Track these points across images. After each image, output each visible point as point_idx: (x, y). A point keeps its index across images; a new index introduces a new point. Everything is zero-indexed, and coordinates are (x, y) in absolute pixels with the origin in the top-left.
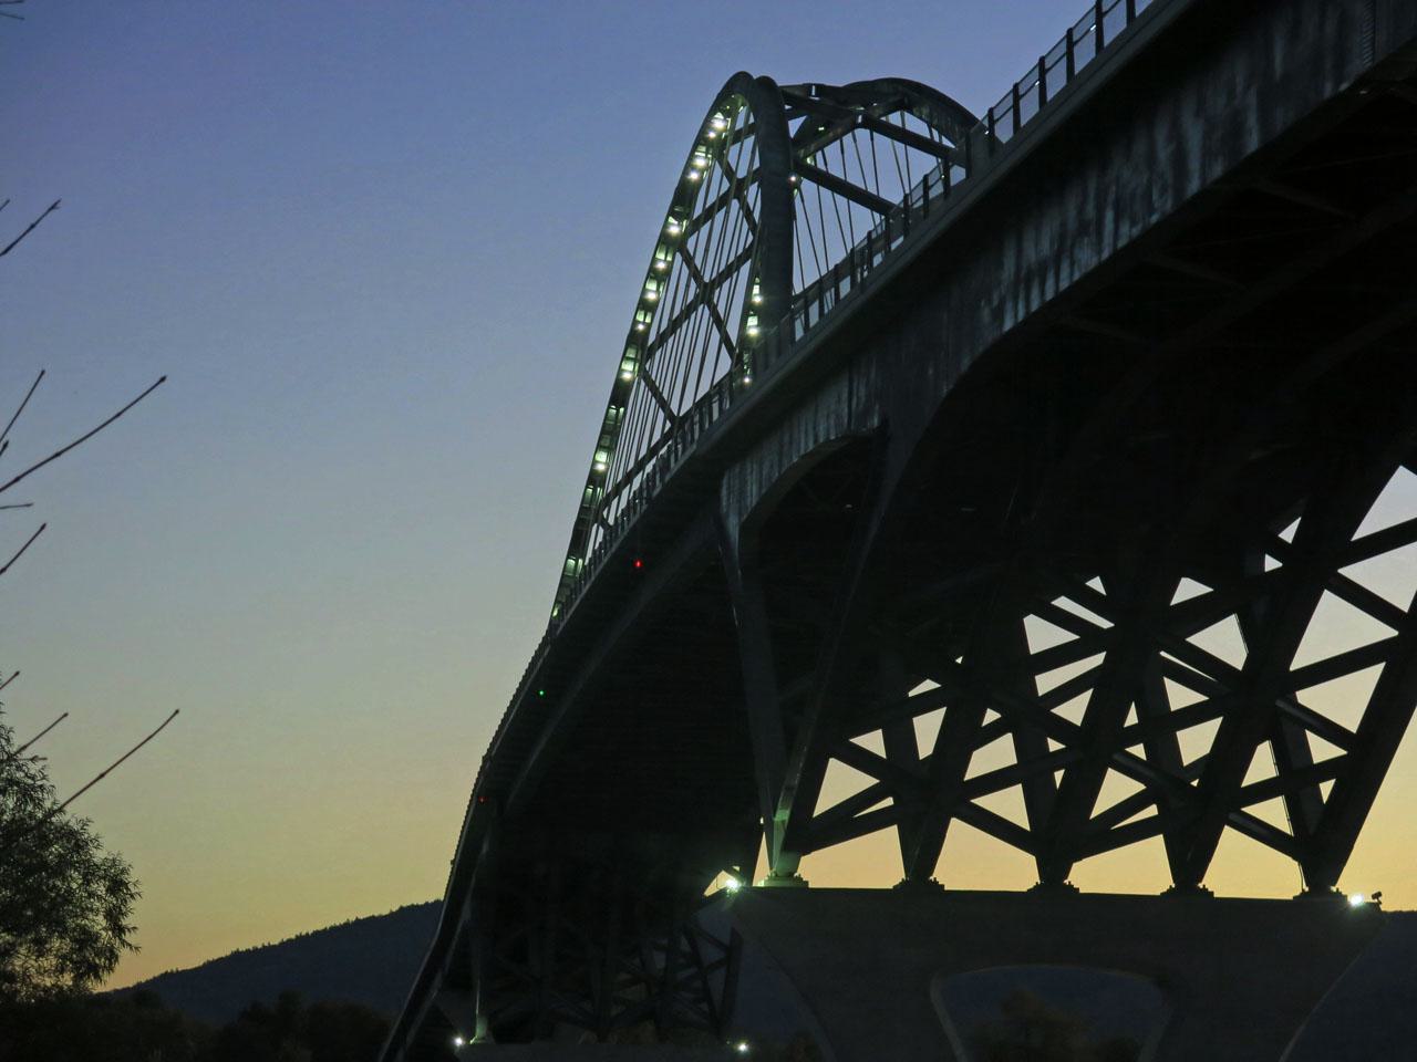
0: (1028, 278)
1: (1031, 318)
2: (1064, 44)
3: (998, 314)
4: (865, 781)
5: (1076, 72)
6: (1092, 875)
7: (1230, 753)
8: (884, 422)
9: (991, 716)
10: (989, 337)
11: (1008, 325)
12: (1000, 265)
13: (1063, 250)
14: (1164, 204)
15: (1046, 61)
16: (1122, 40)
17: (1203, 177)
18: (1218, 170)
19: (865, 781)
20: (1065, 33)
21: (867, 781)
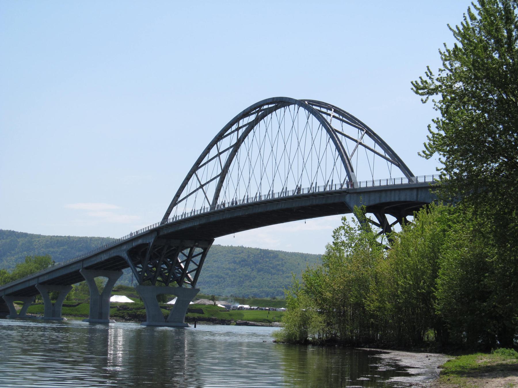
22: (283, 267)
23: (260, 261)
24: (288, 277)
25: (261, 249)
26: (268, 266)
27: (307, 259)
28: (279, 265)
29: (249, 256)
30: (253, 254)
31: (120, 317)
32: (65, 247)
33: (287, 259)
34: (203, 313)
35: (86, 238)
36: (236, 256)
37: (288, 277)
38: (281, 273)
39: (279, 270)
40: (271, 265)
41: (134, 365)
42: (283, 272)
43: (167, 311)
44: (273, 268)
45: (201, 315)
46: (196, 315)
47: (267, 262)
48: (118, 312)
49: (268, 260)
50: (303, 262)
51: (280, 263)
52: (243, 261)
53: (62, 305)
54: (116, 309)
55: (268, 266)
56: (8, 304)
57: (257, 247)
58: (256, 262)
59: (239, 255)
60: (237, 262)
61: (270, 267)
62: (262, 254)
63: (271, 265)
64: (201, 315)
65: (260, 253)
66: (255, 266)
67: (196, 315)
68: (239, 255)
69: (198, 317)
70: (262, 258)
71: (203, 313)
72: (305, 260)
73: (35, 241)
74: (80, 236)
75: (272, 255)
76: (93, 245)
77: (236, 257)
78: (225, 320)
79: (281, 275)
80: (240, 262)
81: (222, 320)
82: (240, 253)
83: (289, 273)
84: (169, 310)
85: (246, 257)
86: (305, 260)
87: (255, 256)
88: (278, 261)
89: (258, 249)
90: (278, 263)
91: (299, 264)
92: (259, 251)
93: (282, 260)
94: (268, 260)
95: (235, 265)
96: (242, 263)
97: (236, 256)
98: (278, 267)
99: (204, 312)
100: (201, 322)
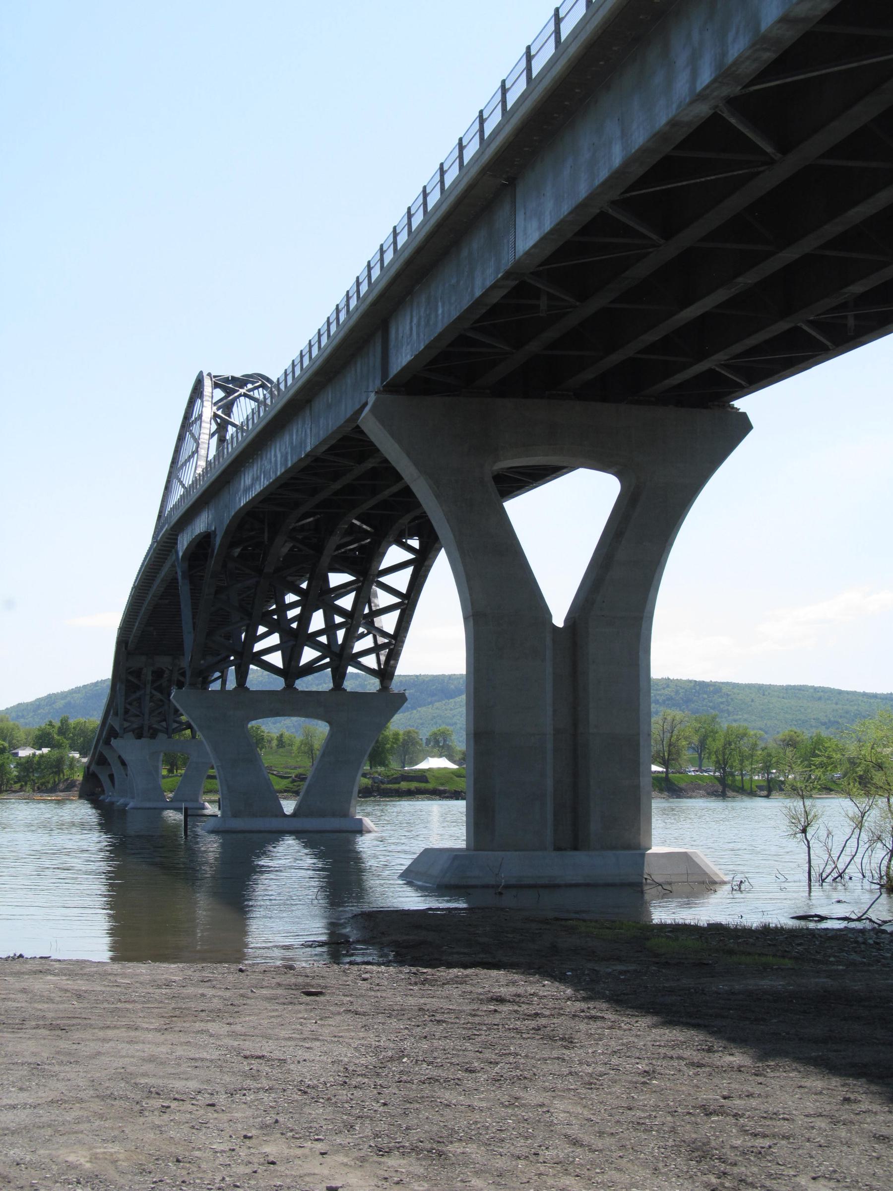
0: (247, 490)
1: (247, 503)
2: (421, 196)
3: (240, 502)
4: (316, 654)
5: (534, 76)
6: (304, 684)
7: (351, 637)
8: (215, 528)
9: (294, 625)
10: (238, 507)
11: (242, 504)
12: (240, 483)
13: (256, 479)
14: (273, 477)
15: (560, 10)
16: (368, 293)
17: (292, 461)
18: (283, 470)
19: (316, 654)
20: (478, 114)
21: (318, 654)
22: (728, 705)
23: (695, 698)
24: (735, 721)
25: (695, 681)
26: (706, 706)
27: (766, 693)
28: (722, 703)
29: (677, 692)
30: (684, 688)
31: (293, 792)
32: (411, 691)
33: (734, 694)
34: (427, 781)
35: (444, 676)
36: (658, 692)
37: (735, 721)
38: (726, 715)
39: (722, 711)
40: (711, 704)
41: (257, 893)
42: (729, 713)
43: (366, 780)
44: (713, 708)
45: (423, 785)
46: (413, 785)
47: (704, 699)
48: (291, 786)
49: (705, 696)
50: (759, 697)
51: (724, 700)
52: (668, 699)
53: (356, 790)
54: (290, 779)
55: (706, 706)
56: (353, 802)
57: (691, 678)
58: (688, 701)
59: (663, 691)
60: (660, 701)
61: (709, 707)
62: (698, 688)
63: (711, 704)
64: (423, 785)
65: (694, 686)
66: (687, 706)
67: (413, 785)
68: (663, 691)
69: (416, 788)
70: (697, 694)
71: (427, 781)
72: (764, 695)
73: (369, 683)
74: (435, 674)
75: (712, 689)
76: (452, 686)
77: (659, 694)
78: (462, 792)
79: (726, 717)
80: (664, 701)
81: (456, 791)
82: (664, 689)
83: (737, 715)
84: (369, 778)
85: (673, 694)
86: (764, 695)
87: (686, 691)
88: (721, 697)
89: (691, 681)
90: (720, 700)
91: (752, 701)
92: (692, 684)
93: (728, 695)
94: (705, 696)
95: (658, 706)
96: (667, 702)
97: (658, 692)
98: (722, 706)
99: (430, 780)
100: (420, 796)
